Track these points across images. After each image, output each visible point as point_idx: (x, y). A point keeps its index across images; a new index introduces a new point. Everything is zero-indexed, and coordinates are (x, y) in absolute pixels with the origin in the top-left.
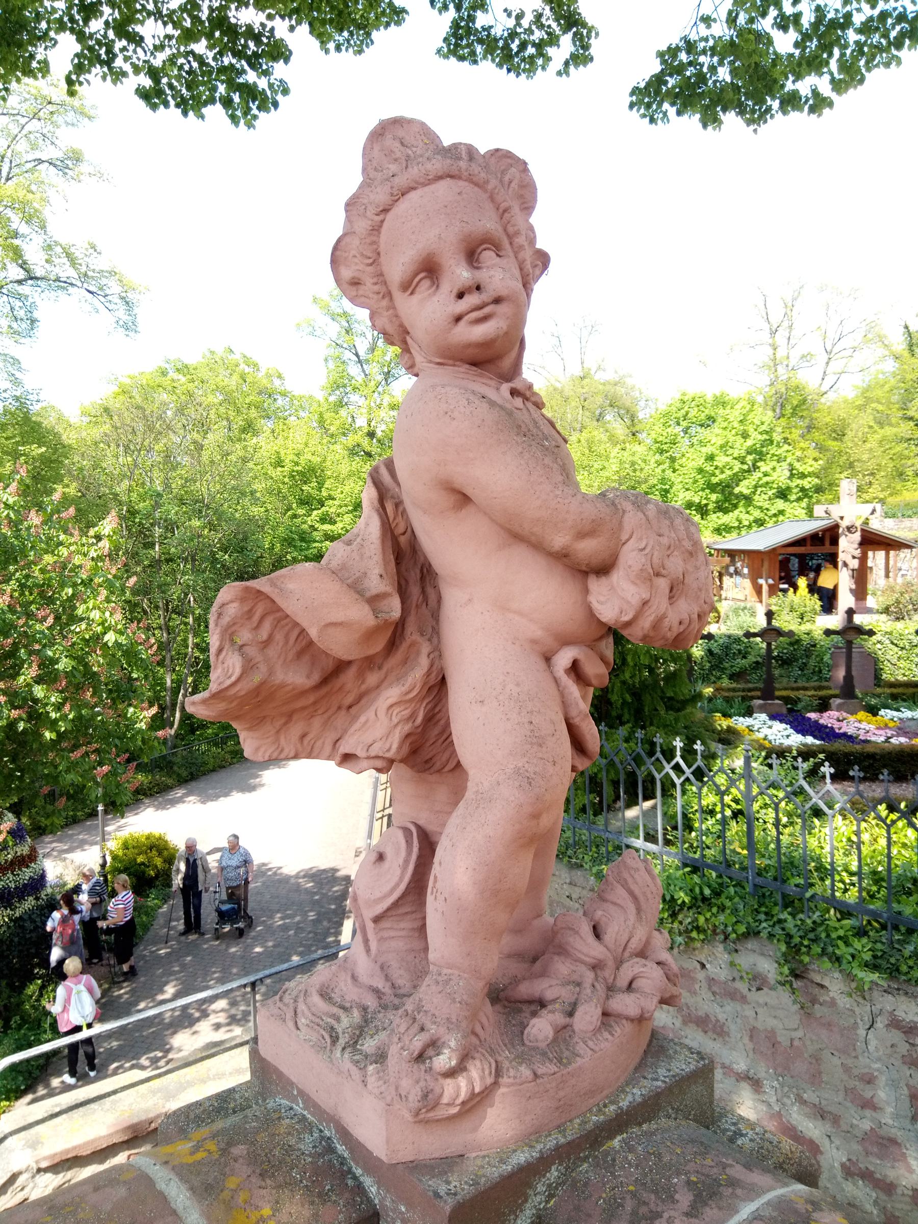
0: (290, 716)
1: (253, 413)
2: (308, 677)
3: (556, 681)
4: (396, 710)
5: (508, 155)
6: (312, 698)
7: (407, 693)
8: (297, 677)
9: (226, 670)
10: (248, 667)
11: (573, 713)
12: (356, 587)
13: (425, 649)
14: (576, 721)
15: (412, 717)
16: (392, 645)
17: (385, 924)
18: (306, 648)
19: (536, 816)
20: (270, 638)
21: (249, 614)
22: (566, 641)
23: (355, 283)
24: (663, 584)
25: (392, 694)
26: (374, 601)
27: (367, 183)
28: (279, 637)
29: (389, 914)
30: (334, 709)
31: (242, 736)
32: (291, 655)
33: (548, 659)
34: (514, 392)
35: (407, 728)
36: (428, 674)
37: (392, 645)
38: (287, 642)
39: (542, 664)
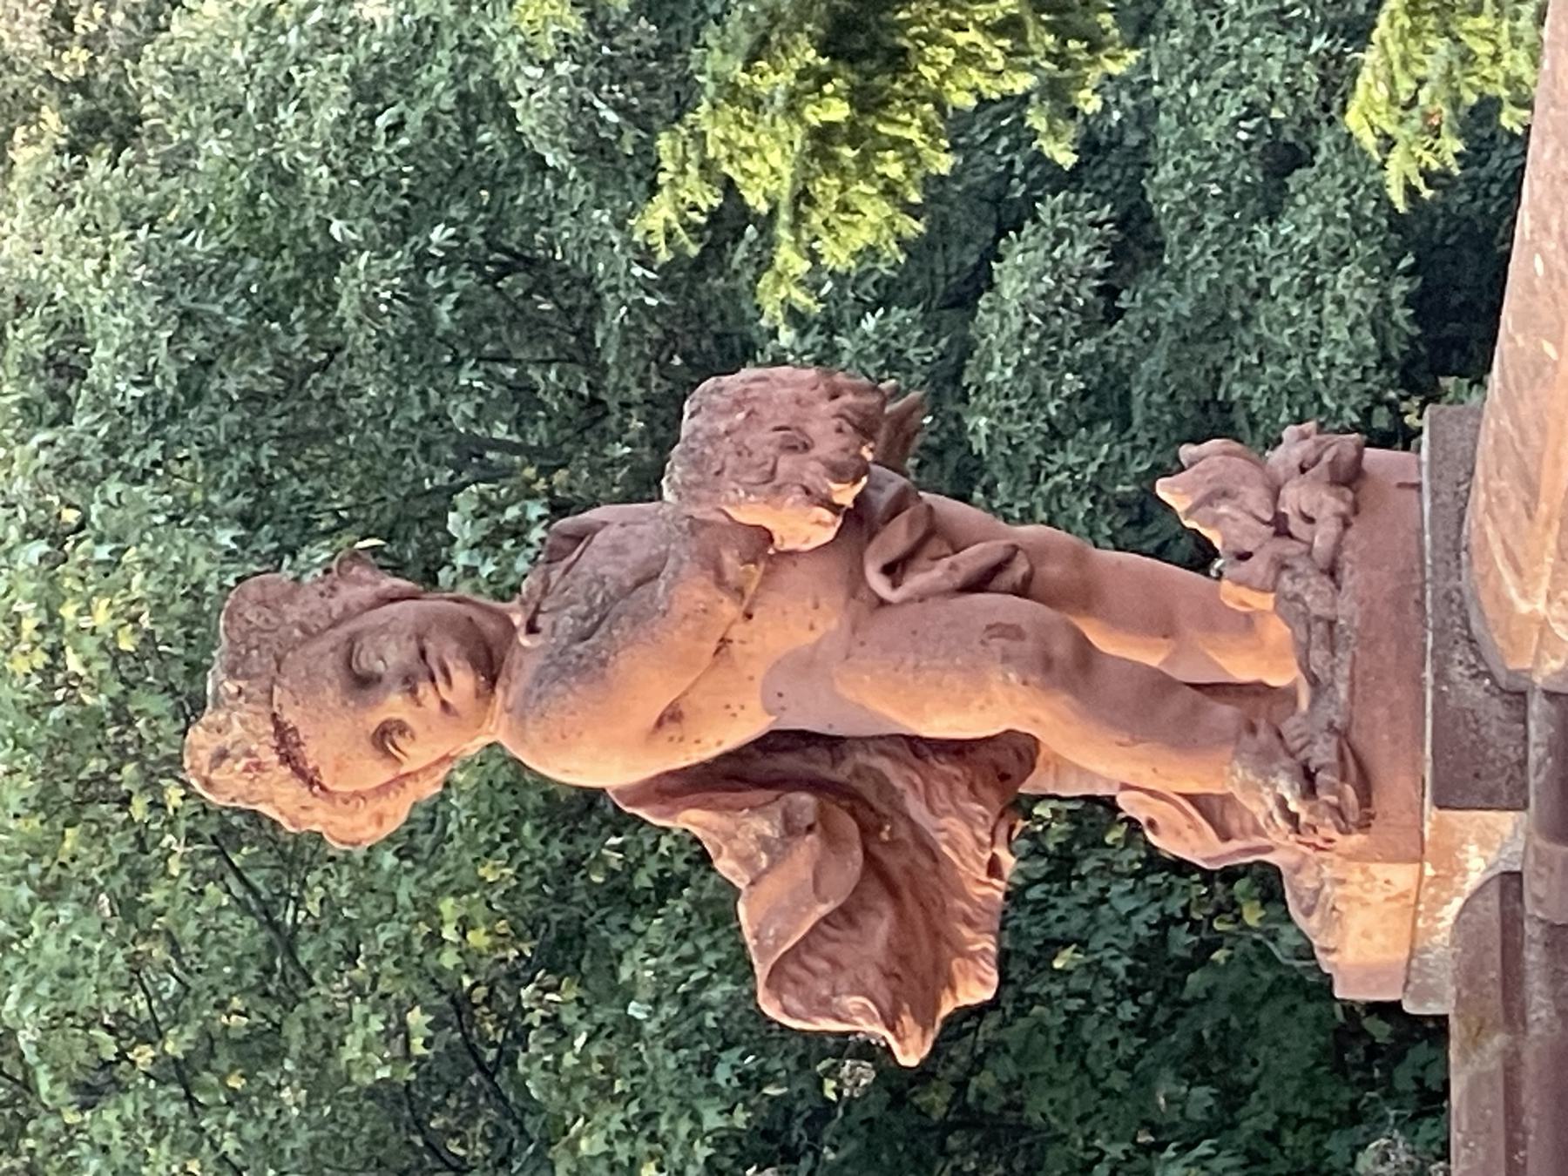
0: (936, 935)
2: (881, 916)
4: (939, 805)
7: (915, 787)
8: (881, 927)
10: (858, 988)
11: (947, 584)
12: (777, 851)
13: (860, 758)
14: (958, 579)
15: (949, 781)
17: (1234, 825)
18: (846, 915)
19: (1047, 663)
21: (796, 981)
22: (857, 579)
24: (786, 464)
25: (915, 808)
26: (791, 829)
28: (829, 948)
29: (1218, 819)
30: (935, 880)
32: (854, 935)
33: (883, 603)
35: (963, 790)
38: (836, 940)
39: (884, 611)
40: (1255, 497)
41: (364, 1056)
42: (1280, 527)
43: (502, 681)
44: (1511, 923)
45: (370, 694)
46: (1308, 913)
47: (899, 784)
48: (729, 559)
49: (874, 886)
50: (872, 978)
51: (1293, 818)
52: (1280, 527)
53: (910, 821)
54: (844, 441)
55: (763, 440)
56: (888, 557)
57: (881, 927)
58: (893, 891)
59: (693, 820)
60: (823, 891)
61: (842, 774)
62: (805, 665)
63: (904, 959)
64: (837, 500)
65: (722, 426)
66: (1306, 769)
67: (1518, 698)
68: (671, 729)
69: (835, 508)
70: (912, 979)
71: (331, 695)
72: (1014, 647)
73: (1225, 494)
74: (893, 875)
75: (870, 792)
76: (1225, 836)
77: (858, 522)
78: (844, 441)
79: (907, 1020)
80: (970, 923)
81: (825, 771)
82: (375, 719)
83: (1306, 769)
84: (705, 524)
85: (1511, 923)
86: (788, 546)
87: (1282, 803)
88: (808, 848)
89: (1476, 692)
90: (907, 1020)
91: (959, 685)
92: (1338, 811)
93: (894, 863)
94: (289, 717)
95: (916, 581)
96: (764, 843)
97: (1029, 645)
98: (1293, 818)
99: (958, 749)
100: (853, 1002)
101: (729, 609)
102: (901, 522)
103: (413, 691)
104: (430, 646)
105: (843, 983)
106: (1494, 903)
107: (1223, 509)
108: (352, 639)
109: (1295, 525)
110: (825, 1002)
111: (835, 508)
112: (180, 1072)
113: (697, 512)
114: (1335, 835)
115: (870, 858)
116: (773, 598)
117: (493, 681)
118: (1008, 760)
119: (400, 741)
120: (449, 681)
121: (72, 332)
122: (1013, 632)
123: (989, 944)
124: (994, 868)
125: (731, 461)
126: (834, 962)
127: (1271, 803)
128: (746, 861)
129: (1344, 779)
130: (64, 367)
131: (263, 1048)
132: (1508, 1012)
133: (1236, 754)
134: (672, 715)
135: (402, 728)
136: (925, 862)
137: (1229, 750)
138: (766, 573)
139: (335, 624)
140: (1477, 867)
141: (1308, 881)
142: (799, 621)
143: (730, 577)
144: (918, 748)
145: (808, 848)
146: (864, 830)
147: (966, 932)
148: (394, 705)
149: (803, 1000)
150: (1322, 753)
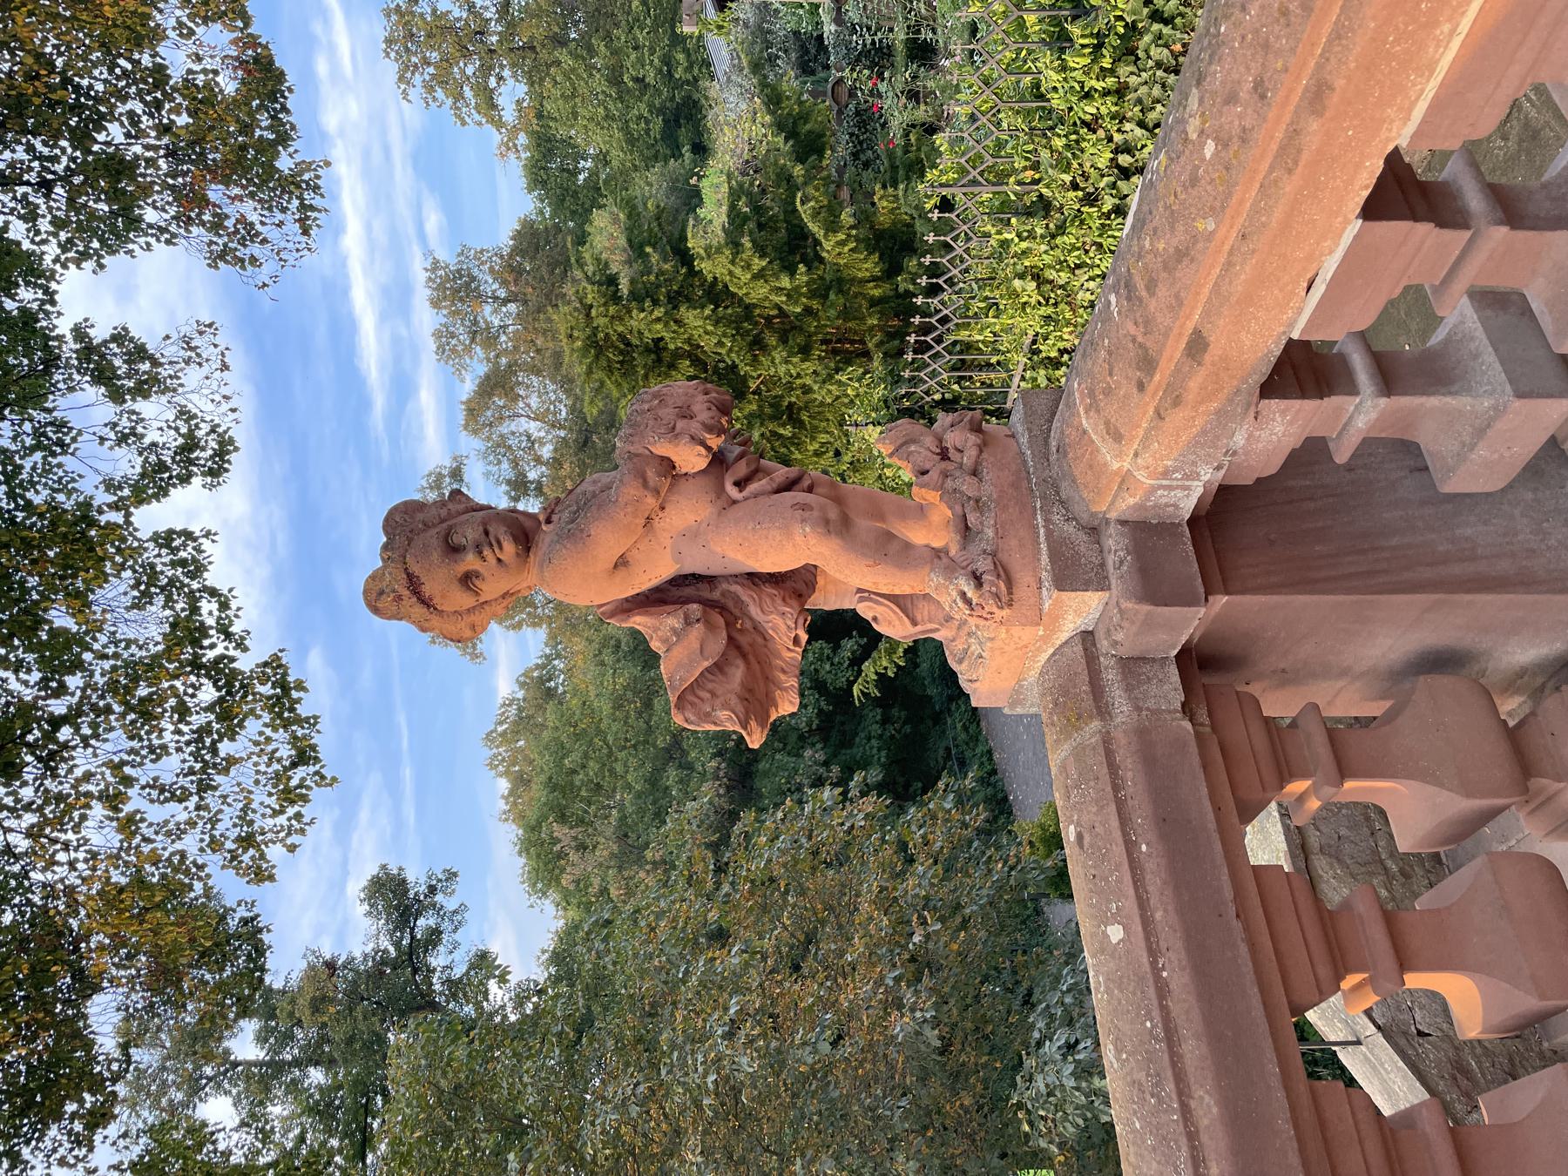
1: (1109, 203)
3: (746, 499)
5: (387, 520)
6: (756, 667)
8: (738, 673)
9: (727, 721)
10: (726, 706)
11: (769, 488)
13: (725, 586)
15: (772, 597)
16: (723, 610)
17: (919, 618)
18: (719, 668)
19: (827, 522)
20: (710, 692)
22: (720, 490)
23: (473, 627)
24: (680, 424)
25: (754, 611)
26: (688, 622)
27: (408, 618)
28: (710, 686)
31: (782, 712)
33: (735, 502)
34: (548, 521)
35: (779, 601)
36: (743, 585)
37: (723, 610)
40: (929, 441)
41: (660, 743)
42: (944, 455)
43: (533, 550)
44: (1091, 658)
45: (457, 556)
46: (960, 661)
47: (745, 598)
48: (651, 474)
49: (733, 653)
50: (734, 701)
51: (968, 602)
52: (944, 455)
53: (751, 619)
54: (711, 414)
55: (668, 413)
56: (736, 478)
57: (738, 673)
58: (744, 656)
59: (639, 622)
60: (706, 654)
61: (716, 595)
62: (691, 535)
63: (750, 691)
64: (709, 443)
65: (646, 407)
66: (974, 573)
67: (1094, 531)
68: (622, 572)
69: (708, 448)
70: (755, 701)
71: (436, 556)
72: (807, 514)
73: (913, 441)
74: (742, 645)
75: (730, 604)
76: (914, 623)
77: (719, 461)
78: (711, 414)
79: (753, 723)
80: (784, 672)
81: (706, 594)
82: (462, 568)
83: (974, 573)
84: (637, 455)
85: (1091, 658)
86: (684, 471)
87: (963, 595)
88: (698, 630)
89: (1070, 528)
90: (753, 723)
91: (778, 538)
92: (997, 596)
93: (743, 640)
94: (415, 569)
95: (753, 487)
96: (674, 630)
97: (816, 513)
98: (968, 602)
99: (776, 579)
100: (723, 714)
101: (651, 501)
102: (743, 462)
103: (480, 553)
104: (491, 529)
105: (718, 702)
106: (1079, 649)
107: (913, 448)
108: (450, 528)
109: (952, 453)
110: (708, 715)
111: (708, 448)
112: (634, 746)
113: (632, 449)
114: (995, 609)
115: (730, 638)
116: (674, 498)
117: (528, 549)
118: (801, 586)
119: (477, 582)
120: (501, 548)
121: (619, 642)
122: (804, 507)
123: (794, 682)
124: (796, 641)
125: (651, 423)
126: (713, 694)
127: (954, 593)
128: (665, 641)
129: (998, 576)
130: (618, 646)
131: (646, 742)
132: (1098, 708)
133: (932, 570)
134: (622, 563)
135: (478, 575)
136: (760, 640)
137: (927, 569)
138: (671, 485)
139: (442, 521)
140: (1070, 626)
141: (959, 646)
142: (688, 511)
143: (651, 484)
144: (754, 578)
145: (699, 628)
146: (727, 624)
147: (783, 677)
148: (470, 561)
149: (698, 715)
150: (983, 565)
